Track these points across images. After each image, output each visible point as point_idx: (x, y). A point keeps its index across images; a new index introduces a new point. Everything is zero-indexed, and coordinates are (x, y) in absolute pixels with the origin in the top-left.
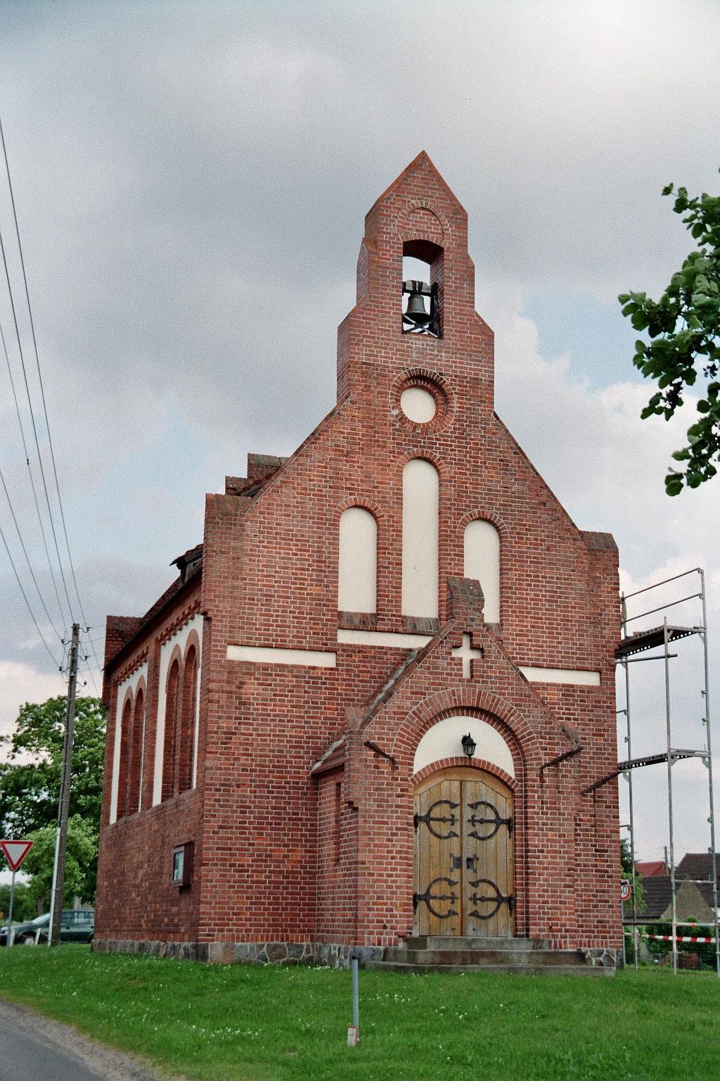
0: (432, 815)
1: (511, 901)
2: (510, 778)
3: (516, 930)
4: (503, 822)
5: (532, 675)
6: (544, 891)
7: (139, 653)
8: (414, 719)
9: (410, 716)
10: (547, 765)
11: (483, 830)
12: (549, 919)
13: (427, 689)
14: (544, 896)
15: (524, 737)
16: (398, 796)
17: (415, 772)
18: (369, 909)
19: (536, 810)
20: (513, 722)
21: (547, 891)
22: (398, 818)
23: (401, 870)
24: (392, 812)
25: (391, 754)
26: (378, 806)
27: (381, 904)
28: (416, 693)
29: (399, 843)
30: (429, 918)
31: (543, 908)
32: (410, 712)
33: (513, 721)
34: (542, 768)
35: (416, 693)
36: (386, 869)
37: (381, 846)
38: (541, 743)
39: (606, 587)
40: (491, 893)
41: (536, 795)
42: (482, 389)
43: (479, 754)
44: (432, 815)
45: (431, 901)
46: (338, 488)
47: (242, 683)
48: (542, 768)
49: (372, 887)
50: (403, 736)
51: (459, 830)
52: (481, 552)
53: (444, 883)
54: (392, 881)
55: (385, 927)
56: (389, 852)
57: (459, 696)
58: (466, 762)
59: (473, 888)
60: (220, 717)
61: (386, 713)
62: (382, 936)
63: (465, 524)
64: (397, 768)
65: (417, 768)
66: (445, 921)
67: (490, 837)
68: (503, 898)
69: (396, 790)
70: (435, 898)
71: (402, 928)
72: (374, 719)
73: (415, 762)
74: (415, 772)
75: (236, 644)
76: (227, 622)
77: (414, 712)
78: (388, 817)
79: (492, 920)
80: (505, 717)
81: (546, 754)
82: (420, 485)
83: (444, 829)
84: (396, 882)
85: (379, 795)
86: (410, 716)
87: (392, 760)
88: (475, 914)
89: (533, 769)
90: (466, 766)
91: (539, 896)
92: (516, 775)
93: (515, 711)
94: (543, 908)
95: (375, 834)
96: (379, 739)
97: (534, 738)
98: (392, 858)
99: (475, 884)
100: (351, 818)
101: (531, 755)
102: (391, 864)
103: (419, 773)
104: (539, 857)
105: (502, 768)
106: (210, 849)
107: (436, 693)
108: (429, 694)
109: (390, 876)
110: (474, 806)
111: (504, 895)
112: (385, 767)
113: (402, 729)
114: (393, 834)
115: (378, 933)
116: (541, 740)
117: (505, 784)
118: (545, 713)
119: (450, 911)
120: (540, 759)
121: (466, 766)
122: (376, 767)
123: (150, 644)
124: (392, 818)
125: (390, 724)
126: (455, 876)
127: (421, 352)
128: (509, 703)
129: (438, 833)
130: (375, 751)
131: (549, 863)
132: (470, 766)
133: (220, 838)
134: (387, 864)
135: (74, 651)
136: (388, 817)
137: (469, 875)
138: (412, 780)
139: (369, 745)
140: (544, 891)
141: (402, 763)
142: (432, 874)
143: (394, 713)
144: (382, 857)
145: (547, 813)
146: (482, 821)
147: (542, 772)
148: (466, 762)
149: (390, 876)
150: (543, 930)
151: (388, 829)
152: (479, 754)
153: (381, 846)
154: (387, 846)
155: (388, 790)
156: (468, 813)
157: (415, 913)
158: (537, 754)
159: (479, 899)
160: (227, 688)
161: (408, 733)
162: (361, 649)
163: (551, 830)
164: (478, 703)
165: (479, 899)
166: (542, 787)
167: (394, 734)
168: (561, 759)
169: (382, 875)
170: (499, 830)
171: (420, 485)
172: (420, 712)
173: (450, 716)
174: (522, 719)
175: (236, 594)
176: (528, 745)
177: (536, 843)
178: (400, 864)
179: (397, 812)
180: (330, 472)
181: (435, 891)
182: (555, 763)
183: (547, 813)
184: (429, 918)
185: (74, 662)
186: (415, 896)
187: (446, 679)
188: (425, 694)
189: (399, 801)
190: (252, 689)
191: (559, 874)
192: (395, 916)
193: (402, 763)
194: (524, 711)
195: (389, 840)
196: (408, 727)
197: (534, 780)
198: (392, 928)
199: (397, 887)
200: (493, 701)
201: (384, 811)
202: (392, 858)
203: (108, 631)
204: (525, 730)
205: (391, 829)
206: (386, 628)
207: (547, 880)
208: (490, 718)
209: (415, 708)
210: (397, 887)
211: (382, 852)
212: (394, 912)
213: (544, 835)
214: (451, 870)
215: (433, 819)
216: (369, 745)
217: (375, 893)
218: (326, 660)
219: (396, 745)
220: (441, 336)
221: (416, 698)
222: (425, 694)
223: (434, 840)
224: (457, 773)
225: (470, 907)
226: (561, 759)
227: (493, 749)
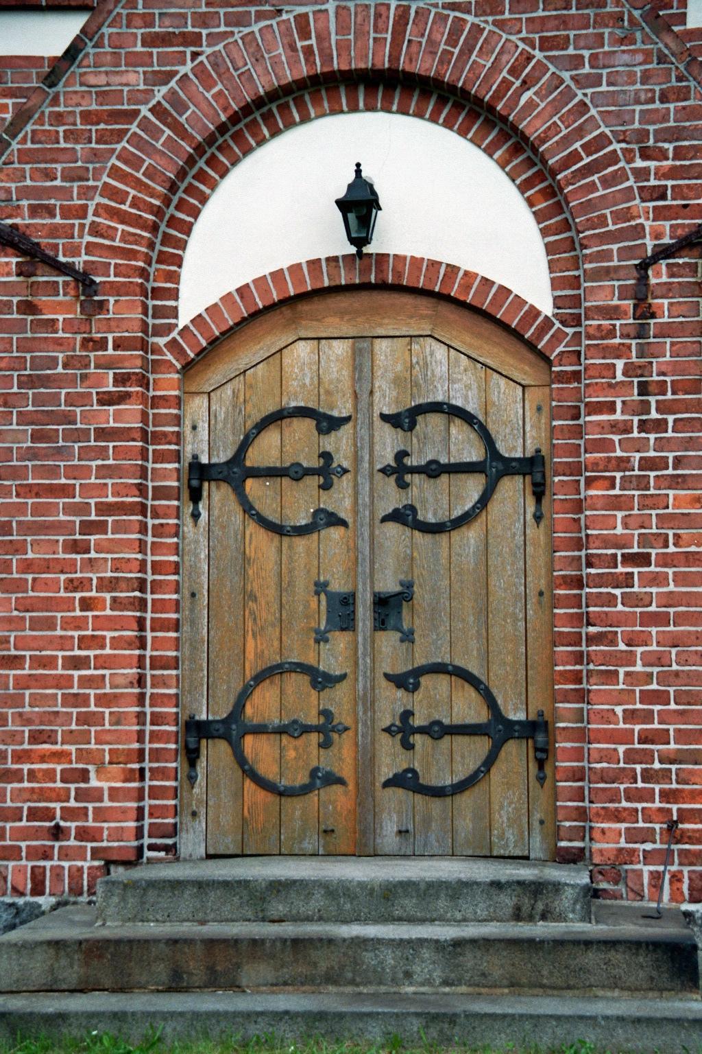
0: (254, 458)
1: (536, 731)
2: (534, 313)
3: (557, 834)
4: (510, 467)
6: (648, 697)
8: (156, 134)
9: (145, 125)
10: (664, 252)
11: (434, 500)
12: (667, 796)
13: (203, 20)
14: (647, 717)
15: (575, 157)
16: (107, 399)
17: (184, 320)
19: (618, 416)
20: (533, 111)
21: (661, 698)
22: (104, 471)
23: (116, 643)
24: (85, 453)
25: (80, 261)
26: (36, 437)
27: (43, 758)
28: (163, 40)
29: (114, 550)
30: (239, 794)
31: (647, 757)
32: (144, 111)
33: (531, 105)
34: (644, 267)
35: (163, 40)
36: (63, 643)
37: (47, 566)
38: (642, 174)
40: (466, 707)
41: (620, 364)
43: (395, 235)
45: (249, 740)
48: (644, 267)
50: (119, 196)
51: (348, 503)
53: (297, 684)
54: (86, 682)
55: (57, 833)
56: (73, 586)
57: (323, 38)
58: (363, 280)
59: (400, 693)
61: (58, 118)
62: (48, 864)
64: (102, 306)
66: (296, 808)
67: (465, 520)
68: (510, 724)
69: (100, 381)
70: (260, 730)
71: (117, 834)
72: (15, 146)
73: (184, 289)
74: (184, 320)
77: (157, 110)
78: (73, 472)
79: (465, 800)
80: (498, 96)
81: (659, 214)
83: (298, 503)
84: (97, 682)
85: (38, 400)
86: (145, 125)
87: (84, 282)
88: (406, 781)
89: (607, 273)
90: (365, 287)
91: (630, 716)
92: (558, 302)
93: (541, 68)
94: (647, 757)
95: (26, 528)
96: (34, 211)
97: (613, 158)
98: (86, 604)
99: (406, 681)
101: (602, 221)
102: (79, 624)
103: (198, 320)
104: (628, 580)
105: (499, 279)
107: (239, 32)
108: (214, 39)
110: (403, 421)
111: (517, 715)
112: (61, 307)
113: (115, 173)
114: (88, 527)
115: (33, 853)
116: (639, 163)
117: (516, 334)
118: (662, 59)
119: (314, 772)
120: (639, 231)
121: (365, 287)
122: (28, 307)
124: (84, 472)
125: (71, 155)
126: (334, 655)
129: (274, 518)
130: (23, 253)
131: (670, 600)
132: (383, 287)
134: (69, 624)
136: (73, 472)
137: (390, 652)
138: (173, 345)
140: (648, 697)
141: (117, 289)
142: (250, 655)
143: (87, 117)
145: (660, 425)
146: (433, 470)
147: (643, 279)
148: (363, 280)
150: (647, 836)
151: (68, 509)
152: (395, 235)
153: (47, 566)
154: (64, 567)
155: (72, 381)
156: (388, 443)
157: (192, 779)
158: (626, 215)
159: (422, 730)
161: (139, 185)
163: (677, 482)
164: (394, 57)
165: (422, 730)
166: (641, 333)
167: (86, 193)
169: (49, 662)
170: (497, 496)
172: (181, 107)
173: (306, 119)
174: (568, 95)
176: (592, 187)
177: (619, 530)
178: (111, 623)
179: (102, 453)
181: (265, 704)
183: (660, 425)
184: (239, 794)
188: (195, 39)
189: (110, 417)
192: (96, 795)
193: (117, 289)
194: (577, 61)
195: (75, 547)
196: (136, 163)
197: (612, 312)
198: (83, 834)
199: (100, 700)
200: (452, 41)
201: (59, 453)
202: (86, 604)
204: (580, 132)
205: (83, 509)
207: (658, 659)
208: (458, 107)
209: (160, 93)
210: (100, 700)
211: (47, 585)
212: (94, 782)
214: (321, 638)
215: (256, 473)
217: (27, 721)
219: (95, 230)
221: (163, 59)
222: (195, 39)
223: (260, 540)
224: (342, 314)
225: (390, 759)
227: (456, 205)
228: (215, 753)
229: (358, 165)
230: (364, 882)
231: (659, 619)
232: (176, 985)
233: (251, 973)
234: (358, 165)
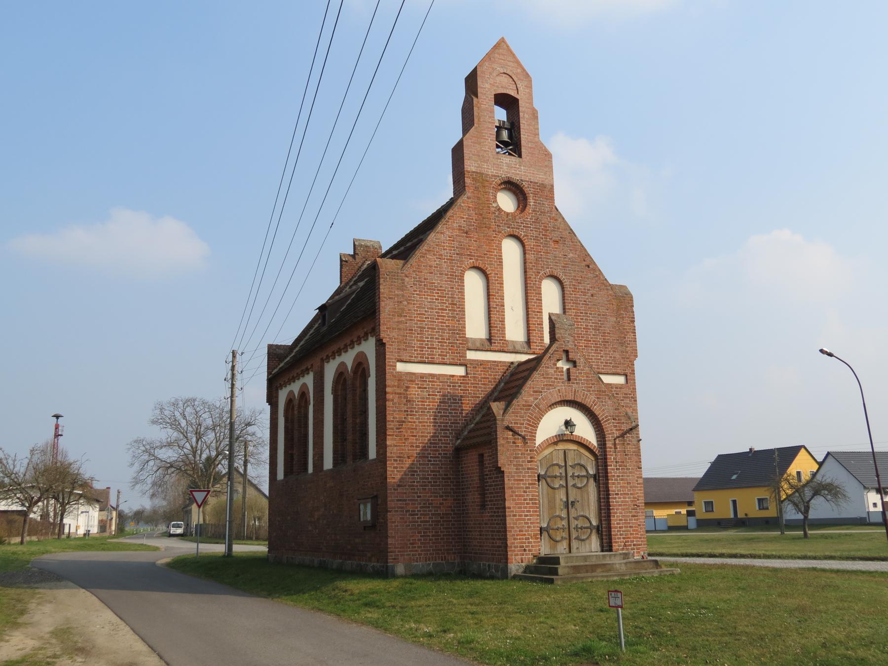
5: (607, 379)
7: (304, 368)
10: (618, 437)
13: (543, 389)
18: (515, 539)
22: (529, 476)
25: (523, 433)
36: (524, 512)
37: (520, 496)
39: (627, 320)
42: (547, 191)
44: (548, 474)
46: (462, 254)
47: (408, 387)
49: (516, 524)
52: (550, 297)
55: (525, 550)
56: (525, 500)
60: (394, 411)
63: (541, 280)
65: (538, 441)
75: (402, 361)
76: (395, 345)
78: (524, 476)
79: (587, 541)
82: (511, 251)
87: (524, 438)
99: (576, 519)
100: (497, 477)
102: (526, 507)
106: (392, 501)
109: (526, 516)
112: (520, 443)
114: (527, 488)
122: (514, 443)
123: (316, 361)
127: (508, 165)
128: (593, 397)
131: (622, 502)
133: (398, 493)
135: (233, 367)
139: (508, 428)
144: (521, 503)
149: (526, 516)
154: (523, 496)
160: (398, 391)
162: (482, 363)
163: (622, 480)
168: (626, 433)
169: (521, 516)
171: (511, 251)
175: (401, 326)
180: (456, 244)
182: (622, 436)
185: (233, 375)
186: (541, 529)
187: (554, 382)
190: (414, 392)
191: (628, 509)
195: (525, 492)
198: (530, 550)
203: (269, 354)
206: (497, 349)
213: (619, 483)
216: (508, 428)
218: (460, 371)
220: (520, 156)
226: (626, 433)
227: (585, 430)
228: (545, 534)
229: (822, 351)
230: (462, 579)
231: (620, 505)
232: (587, 572)
233: (599, 570)
234: (822, 351)
